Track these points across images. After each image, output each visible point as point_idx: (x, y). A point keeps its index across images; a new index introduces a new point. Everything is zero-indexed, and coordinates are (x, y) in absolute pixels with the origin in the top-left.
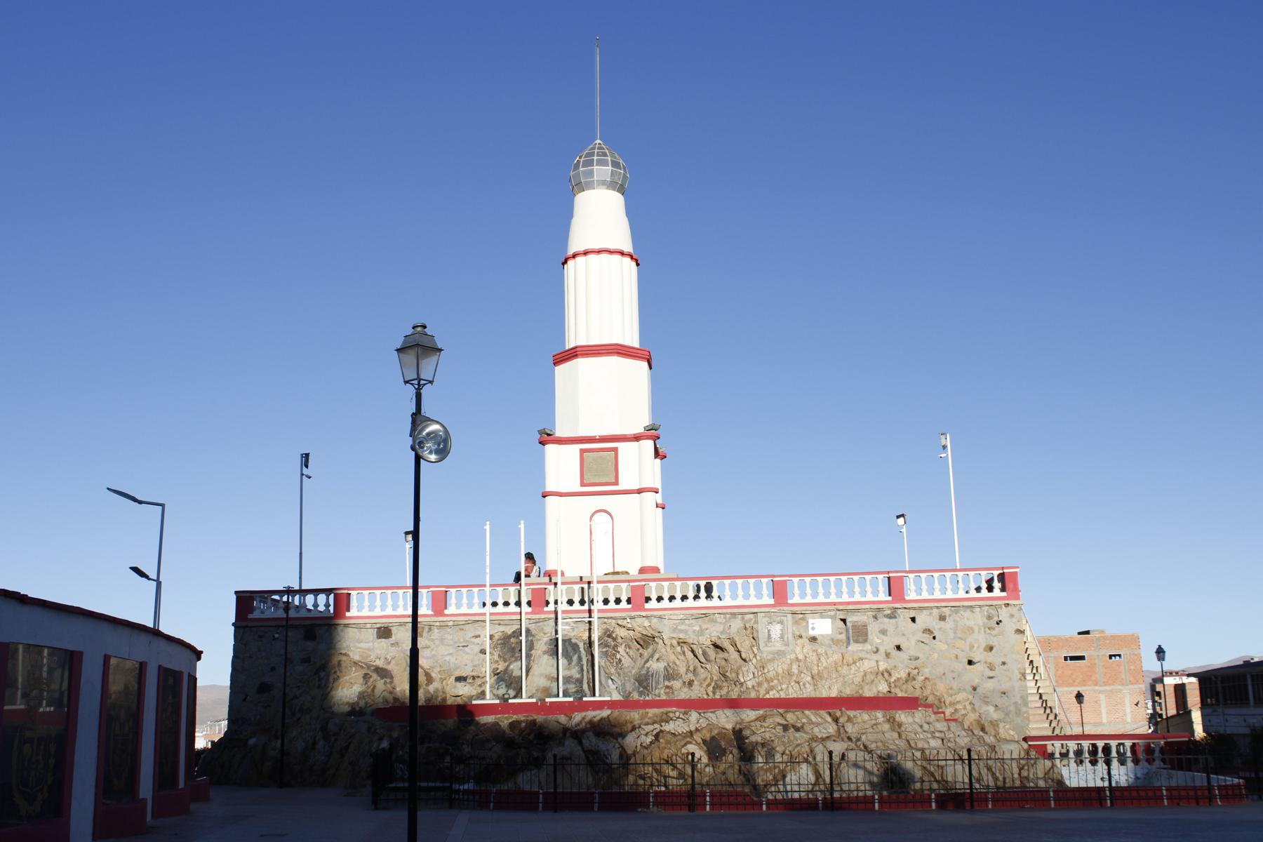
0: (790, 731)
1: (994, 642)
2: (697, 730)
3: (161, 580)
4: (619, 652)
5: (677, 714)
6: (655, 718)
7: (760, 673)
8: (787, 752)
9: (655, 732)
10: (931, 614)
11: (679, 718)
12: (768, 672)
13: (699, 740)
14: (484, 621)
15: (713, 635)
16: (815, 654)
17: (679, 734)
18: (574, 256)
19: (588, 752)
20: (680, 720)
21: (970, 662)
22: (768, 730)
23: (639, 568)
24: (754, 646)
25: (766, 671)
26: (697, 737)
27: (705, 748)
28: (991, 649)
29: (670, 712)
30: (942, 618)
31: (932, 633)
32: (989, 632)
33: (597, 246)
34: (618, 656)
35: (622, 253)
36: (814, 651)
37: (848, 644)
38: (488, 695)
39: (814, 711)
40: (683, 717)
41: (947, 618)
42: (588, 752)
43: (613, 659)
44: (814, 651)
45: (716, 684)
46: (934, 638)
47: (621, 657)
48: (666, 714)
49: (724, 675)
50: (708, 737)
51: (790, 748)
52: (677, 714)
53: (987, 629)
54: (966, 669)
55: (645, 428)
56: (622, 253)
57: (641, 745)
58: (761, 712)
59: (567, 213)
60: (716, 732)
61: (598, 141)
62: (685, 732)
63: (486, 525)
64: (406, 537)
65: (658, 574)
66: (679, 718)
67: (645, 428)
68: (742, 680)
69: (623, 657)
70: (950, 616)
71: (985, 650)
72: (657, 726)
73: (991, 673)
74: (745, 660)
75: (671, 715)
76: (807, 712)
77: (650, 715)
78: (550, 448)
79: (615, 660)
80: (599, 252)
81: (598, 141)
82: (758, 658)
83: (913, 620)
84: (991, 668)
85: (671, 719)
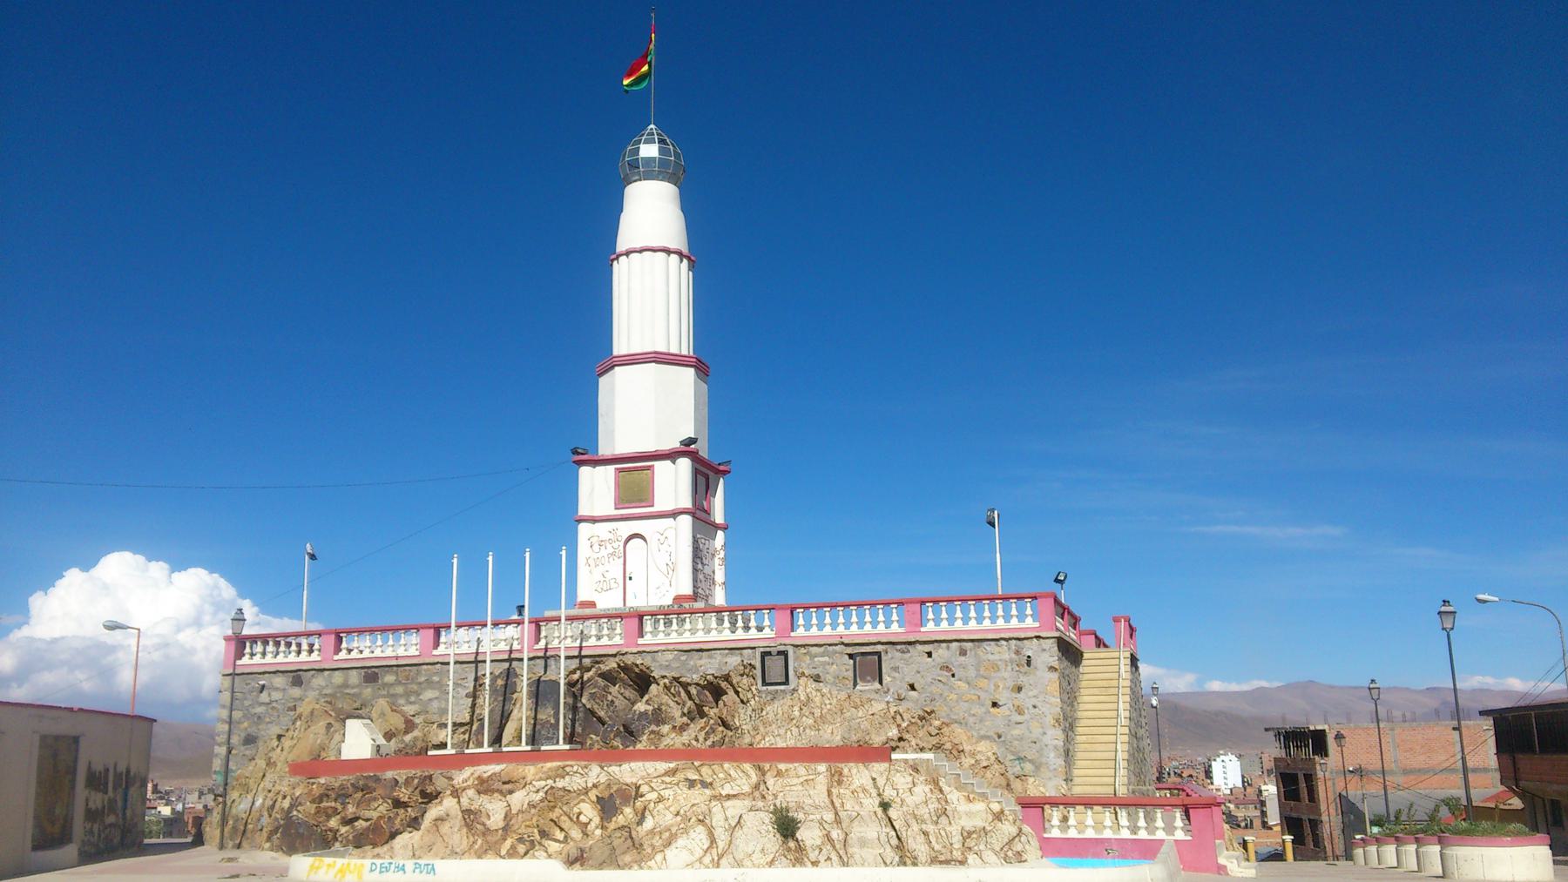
0: (697, 788)
1: (1023, 680)
2: (595, 786)
3: (667, 601)
4: (610, 693)
5: (575, 768)
6: (550, 773)
7: (757, 716)
8: (682, 812)
9: (546, 789)
10: (948, 648)
11: (576, 772)
12: (767, 714)
13: (594, 799)
14: (522, 660)
15: (708, 673)
16: (819, 694)
17: (575, 792)
18: (627, 253)
19: (467, 812)
20: (578, 775)
21: (995, 705)
22: (669, 786)
23: (673, 597)
24: (752, 685)
25: (764, 713)
26: (593, 795)
27: (599, 807)
28: (1020, 689)
29: (567, 766)
30: (963, 653)
31: (951, 670)
32: (1018, 669)
33: (638, 245)
34: (610, 698)
35: (668, 251)
36: (817, 690)
37: (855, 684)
38: (449, 746)
39: (735, 764)
40: (582, 772)
41: (968, 652)
42: (467, 812)
43: (602, 701)
44: (817, 690)
45: (711, 728)
46: (953, 675)
47: (615, 699)
48: (563, 768)
49: (841, 711)
50: (606, 795)
51: (685, 808)
52: (575, 768)
53: (1015, 666)
54: (989, 712)
55: (681, 442)
56: (668, 251)
57: (528, 804)
58: (672, 765)
59: (617, 207)
60: (615, 789)
61: (652, 126)
62: (580, 788)
63: (453, 558)
64: (170, 576)
65: (594, 609)
66: (576, 772)
67: (681, 442)
68: (738, 724)
69: (617, 698)
70: (971, 650)
71: (1012, 690)
72: (550, 782)
73: (1019, 718)
74: (742, 701)
75: (568, 769)
76: (726, 766)
77: (545, 769)
78: (585, 471)
79: (605, 703)
80: (641, 251)
81: (652, 126)
82: (757, 698)
83: (929, 654)
84: (1020, 711)
85: (568, 774)
